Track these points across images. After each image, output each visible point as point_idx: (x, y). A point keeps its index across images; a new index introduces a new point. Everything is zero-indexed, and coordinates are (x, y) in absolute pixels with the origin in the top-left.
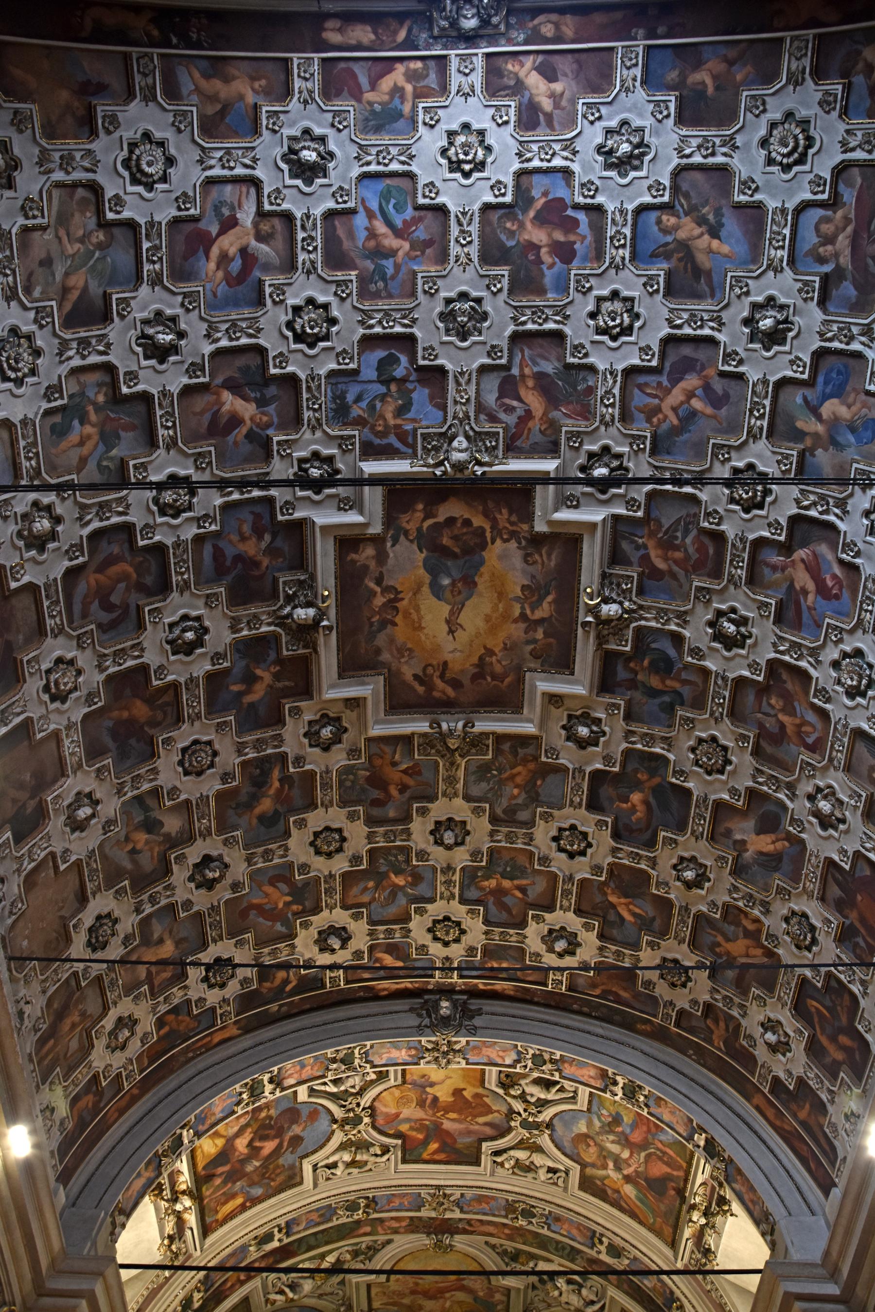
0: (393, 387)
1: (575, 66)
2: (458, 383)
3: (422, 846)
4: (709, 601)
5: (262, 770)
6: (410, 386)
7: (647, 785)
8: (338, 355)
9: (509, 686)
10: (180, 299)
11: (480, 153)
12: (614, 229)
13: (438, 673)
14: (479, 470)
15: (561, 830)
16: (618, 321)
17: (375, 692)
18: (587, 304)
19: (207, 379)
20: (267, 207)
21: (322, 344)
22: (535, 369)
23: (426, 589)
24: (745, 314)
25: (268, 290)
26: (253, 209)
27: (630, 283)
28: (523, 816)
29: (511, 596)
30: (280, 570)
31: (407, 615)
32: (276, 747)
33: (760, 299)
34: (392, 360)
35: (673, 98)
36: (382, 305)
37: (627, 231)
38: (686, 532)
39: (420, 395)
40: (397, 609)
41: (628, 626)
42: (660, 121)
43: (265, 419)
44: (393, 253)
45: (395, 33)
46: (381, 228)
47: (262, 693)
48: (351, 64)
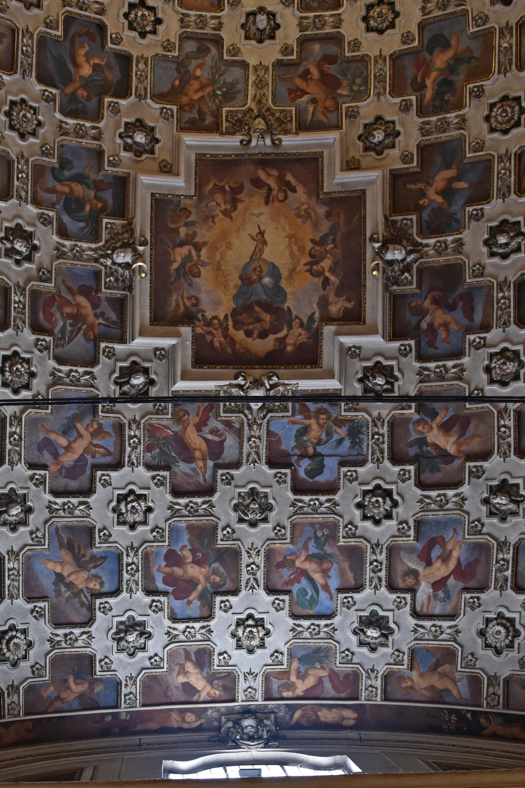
0: (311, 451)
1: (169, 693)
2: (257, 453)
3: (288, 12)
4: (39, 270)
5: (442, 99)
6: (297, 451)
7: (77, 85)
8: (356, 479)
9: (208, 182)
10: (485, 530)
11: (240, 632)
12: (136, 578)
13: (274, 193)
14: (240, 381)
15: (154, 32)
16: (130, 506)
17: (332, 176)
18: (154, 519)
19: (468, 464)
20: (408, 596)
21: (370, 487)
22: (194, 465)
23: (285, 273)
24: (31, 517)
25: (412, 532)
26: (418, 595)
27: (122, 536)
28: (191, 46)
29: (209, 267)
30: (414, 295)
31: (302, 250)
32: (428, 123)
33: (22, 529)
34: (312, 473)
35: (98, 673)
36: (319, 518)
37: (126, 576)
38: (63, 331)
39: (288, 444)
40: (311, 255)
41: (106, 242)
42: (106, 657)
43: (420, 428)
44: (309, 558)
45: (302, 716)
46: (318, 577)
47: (438, 178)
48: (336, 695)
